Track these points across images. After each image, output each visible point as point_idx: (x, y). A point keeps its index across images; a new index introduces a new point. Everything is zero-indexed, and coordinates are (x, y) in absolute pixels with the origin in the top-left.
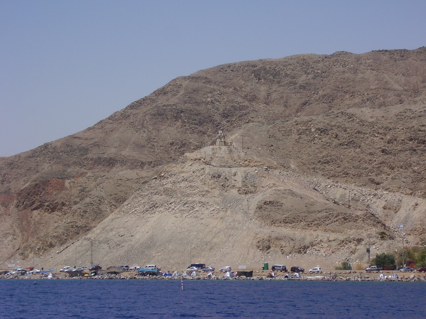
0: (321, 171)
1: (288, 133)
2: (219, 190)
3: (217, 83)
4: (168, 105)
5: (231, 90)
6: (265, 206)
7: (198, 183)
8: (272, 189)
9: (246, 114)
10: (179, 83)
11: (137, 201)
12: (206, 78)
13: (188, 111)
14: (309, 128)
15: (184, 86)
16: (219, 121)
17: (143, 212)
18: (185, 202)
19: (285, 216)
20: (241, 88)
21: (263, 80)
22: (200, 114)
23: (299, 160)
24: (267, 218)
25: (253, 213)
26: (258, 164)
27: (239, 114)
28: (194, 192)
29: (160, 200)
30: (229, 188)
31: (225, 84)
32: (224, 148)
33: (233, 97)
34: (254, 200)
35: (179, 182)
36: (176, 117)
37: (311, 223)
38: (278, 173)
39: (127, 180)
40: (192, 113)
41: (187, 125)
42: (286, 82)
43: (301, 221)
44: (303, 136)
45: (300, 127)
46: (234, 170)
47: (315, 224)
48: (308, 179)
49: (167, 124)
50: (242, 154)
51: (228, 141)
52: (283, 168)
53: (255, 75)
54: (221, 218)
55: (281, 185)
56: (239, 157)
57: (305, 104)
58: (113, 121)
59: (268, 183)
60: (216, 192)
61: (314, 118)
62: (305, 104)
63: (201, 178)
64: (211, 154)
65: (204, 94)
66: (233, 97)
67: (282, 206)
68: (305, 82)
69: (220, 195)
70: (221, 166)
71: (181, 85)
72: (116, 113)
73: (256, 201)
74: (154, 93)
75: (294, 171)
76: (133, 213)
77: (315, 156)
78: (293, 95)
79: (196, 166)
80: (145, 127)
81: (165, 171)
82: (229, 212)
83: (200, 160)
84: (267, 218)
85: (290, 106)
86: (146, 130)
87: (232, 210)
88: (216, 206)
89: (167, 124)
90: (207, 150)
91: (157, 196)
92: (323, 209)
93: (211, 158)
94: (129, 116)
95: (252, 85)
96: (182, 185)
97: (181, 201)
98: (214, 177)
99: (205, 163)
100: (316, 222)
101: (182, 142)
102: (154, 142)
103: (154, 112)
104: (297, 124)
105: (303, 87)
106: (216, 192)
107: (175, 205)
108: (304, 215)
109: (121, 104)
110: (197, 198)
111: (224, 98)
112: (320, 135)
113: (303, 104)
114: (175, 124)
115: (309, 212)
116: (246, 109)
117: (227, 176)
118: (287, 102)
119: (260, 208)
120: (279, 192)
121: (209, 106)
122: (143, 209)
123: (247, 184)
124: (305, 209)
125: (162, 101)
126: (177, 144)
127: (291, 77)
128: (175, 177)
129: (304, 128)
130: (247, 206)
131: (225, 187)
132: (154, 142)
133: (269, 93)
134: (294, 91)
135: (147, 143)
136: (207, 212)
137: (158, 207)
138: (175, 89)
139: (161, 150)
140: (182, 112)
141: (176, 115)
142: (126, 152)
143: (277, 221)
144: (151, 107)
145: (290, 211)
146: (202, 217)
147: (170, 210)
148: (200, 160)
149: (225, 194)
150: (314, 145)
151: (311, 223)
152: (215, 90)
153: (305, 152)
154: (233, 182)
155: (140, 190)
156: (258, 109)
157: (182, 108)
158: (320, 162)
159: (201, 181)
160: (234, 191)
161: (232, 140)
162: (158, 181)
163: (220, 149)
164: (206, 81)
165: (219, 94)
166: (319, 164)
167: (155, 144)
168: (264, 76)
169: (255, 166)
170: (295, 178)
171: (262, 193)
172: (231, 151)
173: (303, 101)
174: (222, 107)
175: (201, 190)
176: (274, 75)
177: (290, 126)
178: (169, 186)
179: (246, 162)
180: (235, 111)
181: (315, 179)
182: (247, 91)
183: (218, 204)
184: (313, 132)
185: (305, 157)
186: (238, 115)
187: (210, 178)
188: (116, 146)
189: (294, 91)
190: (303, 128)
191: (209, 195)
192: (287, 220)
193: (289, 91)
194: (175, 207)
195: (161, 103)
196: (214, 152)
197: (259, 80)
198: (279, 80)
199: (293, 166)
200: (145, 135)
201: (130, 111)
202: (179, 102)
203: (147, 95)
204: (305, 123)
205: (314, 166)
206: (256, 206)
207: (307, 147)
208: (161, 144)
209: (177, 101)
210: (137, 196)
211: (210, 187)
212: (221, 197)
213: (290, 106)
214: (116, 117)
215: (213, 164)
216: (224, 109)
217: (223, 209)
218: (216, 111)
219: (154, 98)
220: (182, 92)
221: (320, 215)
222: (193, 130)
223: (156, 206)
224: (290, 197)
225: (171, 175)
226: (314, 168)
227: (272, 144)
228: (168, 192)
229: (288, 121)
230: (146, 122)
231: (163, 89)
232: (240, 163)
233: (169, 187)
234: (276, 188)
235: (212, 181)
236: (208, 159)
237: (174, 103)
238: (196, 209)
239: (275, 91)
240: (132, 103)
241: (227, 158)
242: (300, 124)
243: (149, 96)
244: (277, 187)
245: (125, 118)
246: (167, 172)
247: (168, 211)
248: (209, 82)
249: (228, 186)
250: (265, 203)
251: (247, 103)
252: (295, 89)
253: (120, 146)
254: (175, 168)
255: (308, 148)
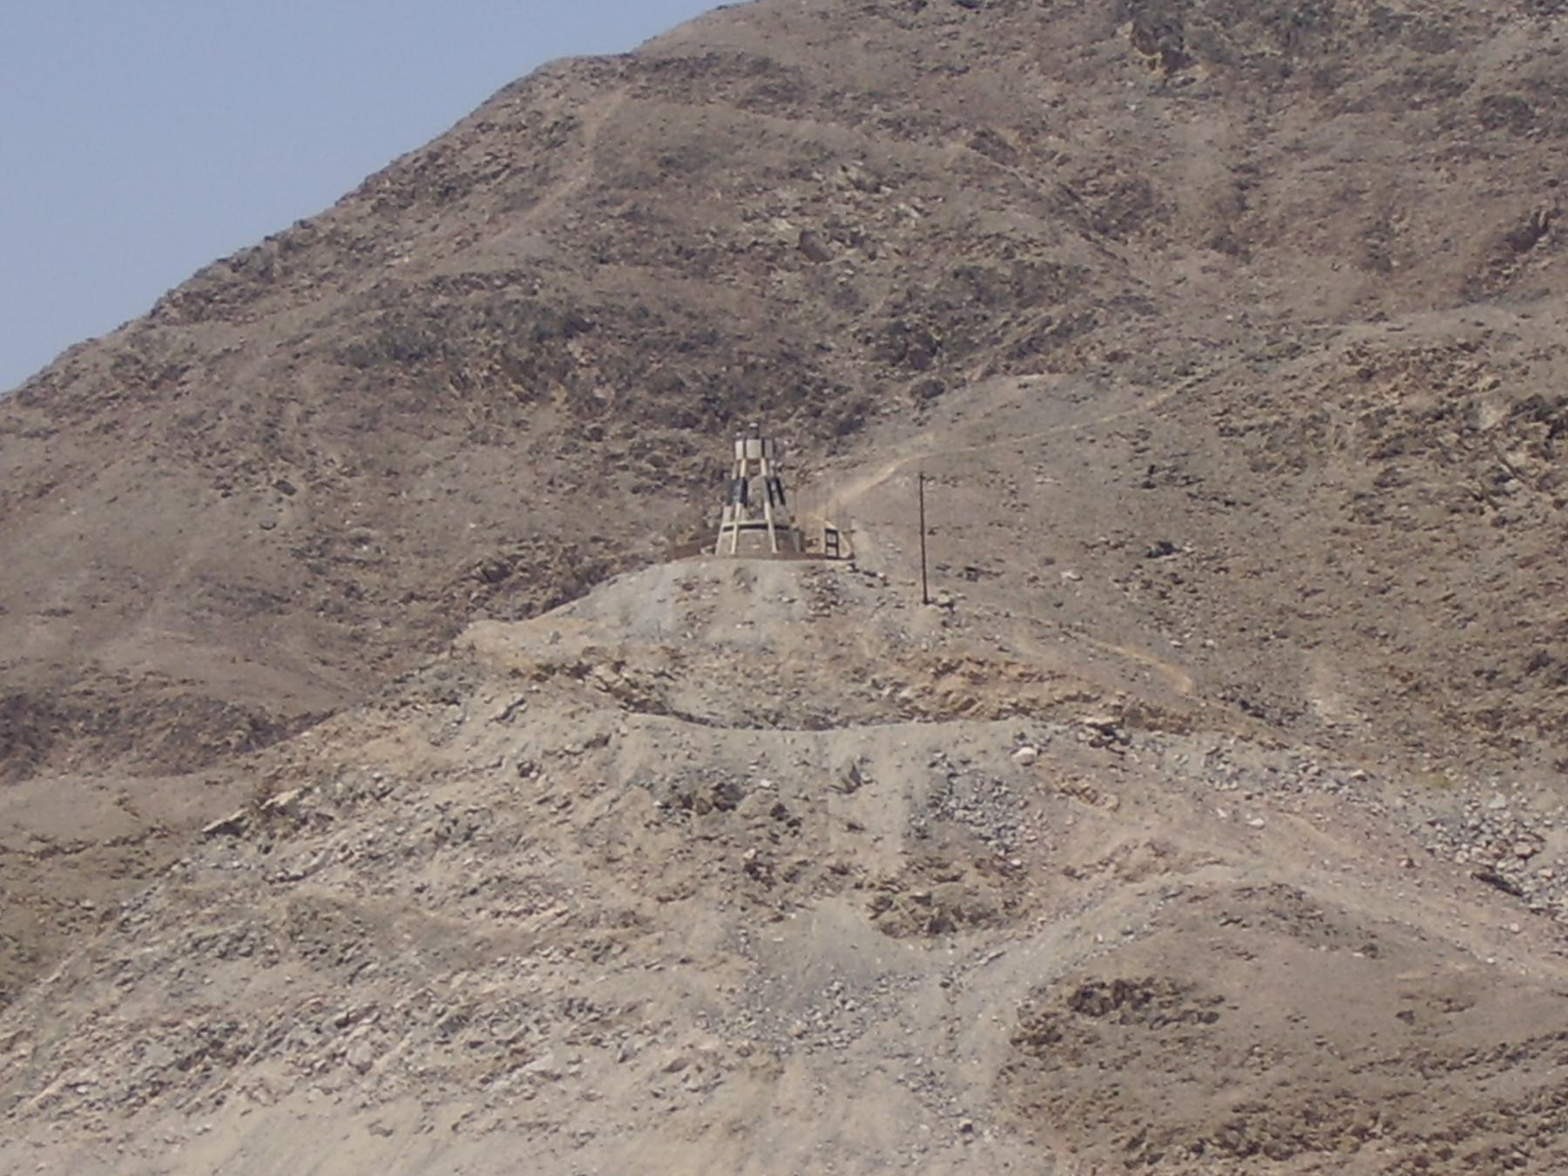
0: (1553, 736)
1: (1294, 446)
2: (723, 907)
3: (847, 102)
4: (467, 282)
5: (955, 148)
6: (1085, 1021)
7: (561, 860)
8: (1138, 887)
9: (1064, 333)
10: (550, 107)
11: (85, 1010)
12: (763, 66)
13: (621, 324)
14: (1461, 402)
15: (591, 131)
16: (858, 392)
17: (131, 1100)
18: (453, 1010)
19: (1235, 1096)
20: (1032, 130)
21: (1200, 72)
22: (712, 339)
23: (1377, 655)
24: (1095, 1114)
25: (987, 1078)
26: (1043, 692)
27: (1016, 331)
28: (528, 924)
29: (264, 996)
30: (802, 885)
31: (904, 108)
32: (777, 574)
33: (965, 204)
34: (999, 975)
35: (409, 853)
36: (523, 370)
37: (1440, 1146)
38: (1197, 764)
39: (43, 855)
40: (651, 333)
41: (615, 429)
42: (1382, 76)
43: (1363, 1133)
44: (1411, 466)
45: (1392, 400)
46: (843, 746)
47: (1471, 1159)
48: (1443, 804)
49: (462, 424)
50: (920, 621)
51: (816, 519)
52: (1243, 723)
53: (1138, 34)
54: (734, 1129)
55: (1219, 853)
56: (895, 642)
57: (1521, 242)
58: (57, 413)
59: (1116, 843)
60: (703, 923)
61: (1505, 326)
62: (1521, 242)
63: (585, 812)
64: (668, 623)
65: (749, 188)
66: (965, 204)
67: (1212, 1018)
68: (1525, 71)
69: (735, 942)
70: (751, 720)
71: (569, 125)
72: (76, 350)
73: (1011, 981)
74: (365, 190)
75: (1332, 739)
76: (55, 1110)
77: (1505, 620)
78: (1435, 178)
79: (547, 724)
80: (286, 454)
81: (303, 773)
82: (794, 1082)
83: (580, 671)
84: (1095, 1114)
85: (1410, 261)
86: (295, 478)
87: (818, 1060)
88: (694, 1034)
89: (462, 424)
90: (646, 597)
91: (240, 966)
92: (1539, 1033)
93: (675, 656)
94: (173, 373)
95: (1119, 107)
96: (436, 872)
97: (423, 1000)
98: (687, 802)
99: (618, 694)
100: (1479, 1143)
101: (571, 557)
102: (363, 564)
103: (358, 339)
104: (1367, 375)
105: (1510, 113)
106: (703, 923)
107: (378, 1036)
108: (1388, 1085)
109: (109, 291)
110: (547, 978)
111: (899, 216)
112: (1547, 457)
113: (1510, 238)
114: (518, 424)
115: (1429, 1064)
116: (1069, 292)
117: (785, 796)
118: (1383, 229)
119: (1041, 1038)
120: (1197, 911)
121: (786, 280)
122: (126, 1079)
123: (946, 856)
124: (1396, 1038)
125: (423, 247)
126: (535, 574)
127: (1416, 41)
128: (383, 813)
129: (1421, 401)
130: (943, 1030)
131: (770, 884)
132: (363, 564)
133: (1248, 169)
134: (1443, 144)
135: (305, 575)
136: (622, 1083)
137: (242, 1052)
138: (526, 159)
139: (413, 626)
140: (573, 327)
141: (524, 354)
142: (138, 652)
143: (1168, 1137)
144: (343, 300)
145: (1279, 1057)
146: (581, 1124)
147: (336, 1077)
148: (580, 671)
149: (773, 934)
150: (1495, 534)
151: (1440, 1146)
152: (827, 157)
153: (1423, 594)
154: (838, 838)
155: (110, 926)
156: (1164, 290)
157: (572, 299)
158: (1538, 663)
159: (584, 837)
160: (847, 914)
161: (842, 515)
162: (251, 850)
163: (745, 581)
164: (765, 90)
165: (859, 185)
166: (1537, 681)
167: (369, 580)
168: (1209, 38)
169: (1019, 710)
170: (1330, 800)
171: (1067, 923)
172: (828, 599)
173: (1507, 216)
174: (887, 283)
175: (584, 906)
176: (1284, 24)
177: (1309, 394)
178: (333, 885)
179: (953, 682)
180: (982, 310)
181: (1500, 801)
182: (1075, 152)
183: (711, 1019)
184: (1491, 433)
185: (1424, 629)
186: (1008, 341)
187: (653, 816)
188: (60, 604)
189: (1443, 144)
190: (1413, 401)
191: (640, 945)
192: (1252, 1133)
193: (1398, 148)
194: (380, 1049)
195: (421, 267)
196: (693, 606)
197: (1170, 72)
198: (1323, 61)
199: (1324, 706)
200: (286, 516)
201: (180, 336)
202: (549, 251)
203: (309, 212)
204: (1423, 366)
205: (1492, 698)
206: (1014, 1024)
207: (1442, 547)
208: (409, 579)
209: (534, 246)
210: (83, 972)
211: (652, 884)
212: (738, 962)
213: (1410, 261)
214: (79, 387)
215: (688, 701)
216: (901, 297)
217: (746, 1053)
218: (835, 317)
219: (361, 230)
220: (577, 176)
221: (1510, 1084)
222: (656, 462)
223: (230, 1045)
224: (1282, 945)
225: (349, 802)
226: (1493, 718)
227: (1163, 532)
228: (324, 938)
229: (1294, 351)
230: (294, 410)
231: (433, 157)
232: (899, 686)
233: (330, 893)
234: (1171, 880)
235: (671, 838)
236: (645, 665)
237: (509, 265)
238: (536, 1066)
239: (1297, 148)
240: (201, 274)
241: (798, 652)
242: (1392, 371)
243: (327, 217)
244: (1183, 868)
245: (143, 389)
246: (323, 777)
247: (325, 1081)
248: (785, 91)
249: (791, 877)
250: (1082, 1000)
251: (1073, 248)
252: (1447, 125)
253: (92, 602)
254: (381, 745)
255: (1452, 561)
